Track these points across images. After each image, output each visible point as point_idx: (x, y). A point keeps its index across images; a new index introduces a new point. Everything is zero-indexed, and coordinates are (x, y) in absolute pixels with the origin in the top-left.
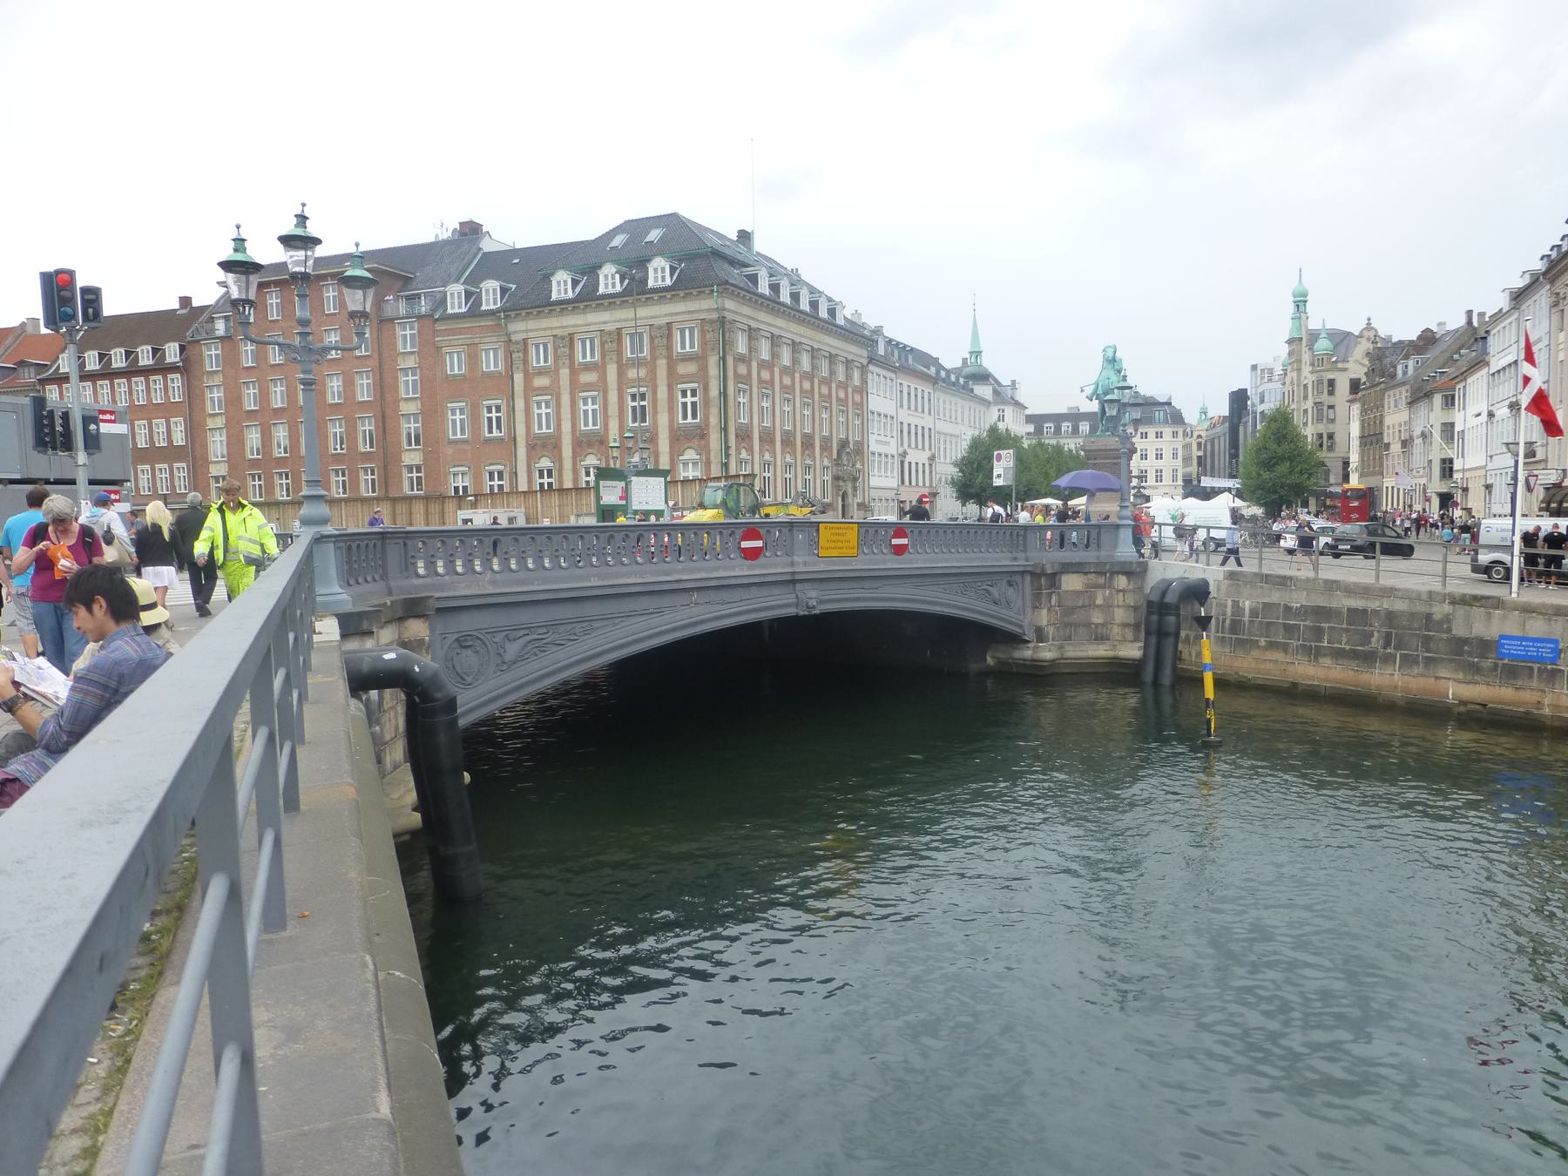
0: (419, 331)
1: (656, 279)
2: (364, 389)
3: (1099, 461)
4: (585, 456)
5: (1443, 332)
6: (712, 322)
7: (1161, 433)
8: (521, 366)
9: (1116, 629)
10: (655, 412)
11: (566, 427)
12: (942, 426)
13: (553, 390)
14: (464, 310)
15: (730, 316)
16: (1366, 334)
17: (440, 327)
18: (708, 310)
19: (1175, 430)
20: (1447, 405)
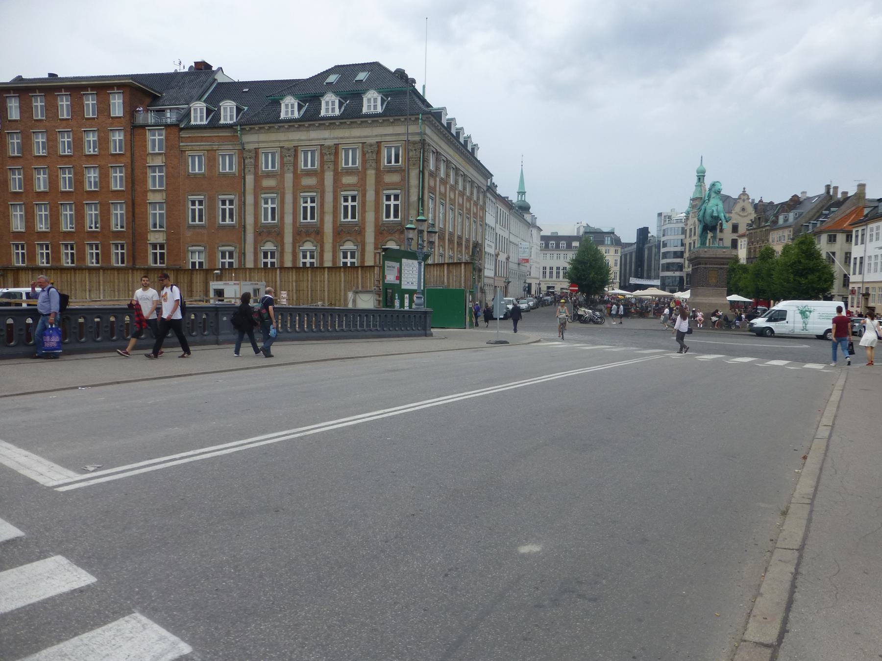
0: (166, 137)
1: (369, 107)
2: (117, 180)
3: (708, 266)
4: (304, 243)
5: (805, 198)
6: (414, 143)
7: (609, 250)
8: (252, 170)
10: (364, 211)
11: (288, 219)
12: (513, 239)
13: (280, 190)
14: (205, 122)
15: (428, 140)
16: (742, 197)
17: (184, 134)
19: (617, 249)
20: (830, 241)
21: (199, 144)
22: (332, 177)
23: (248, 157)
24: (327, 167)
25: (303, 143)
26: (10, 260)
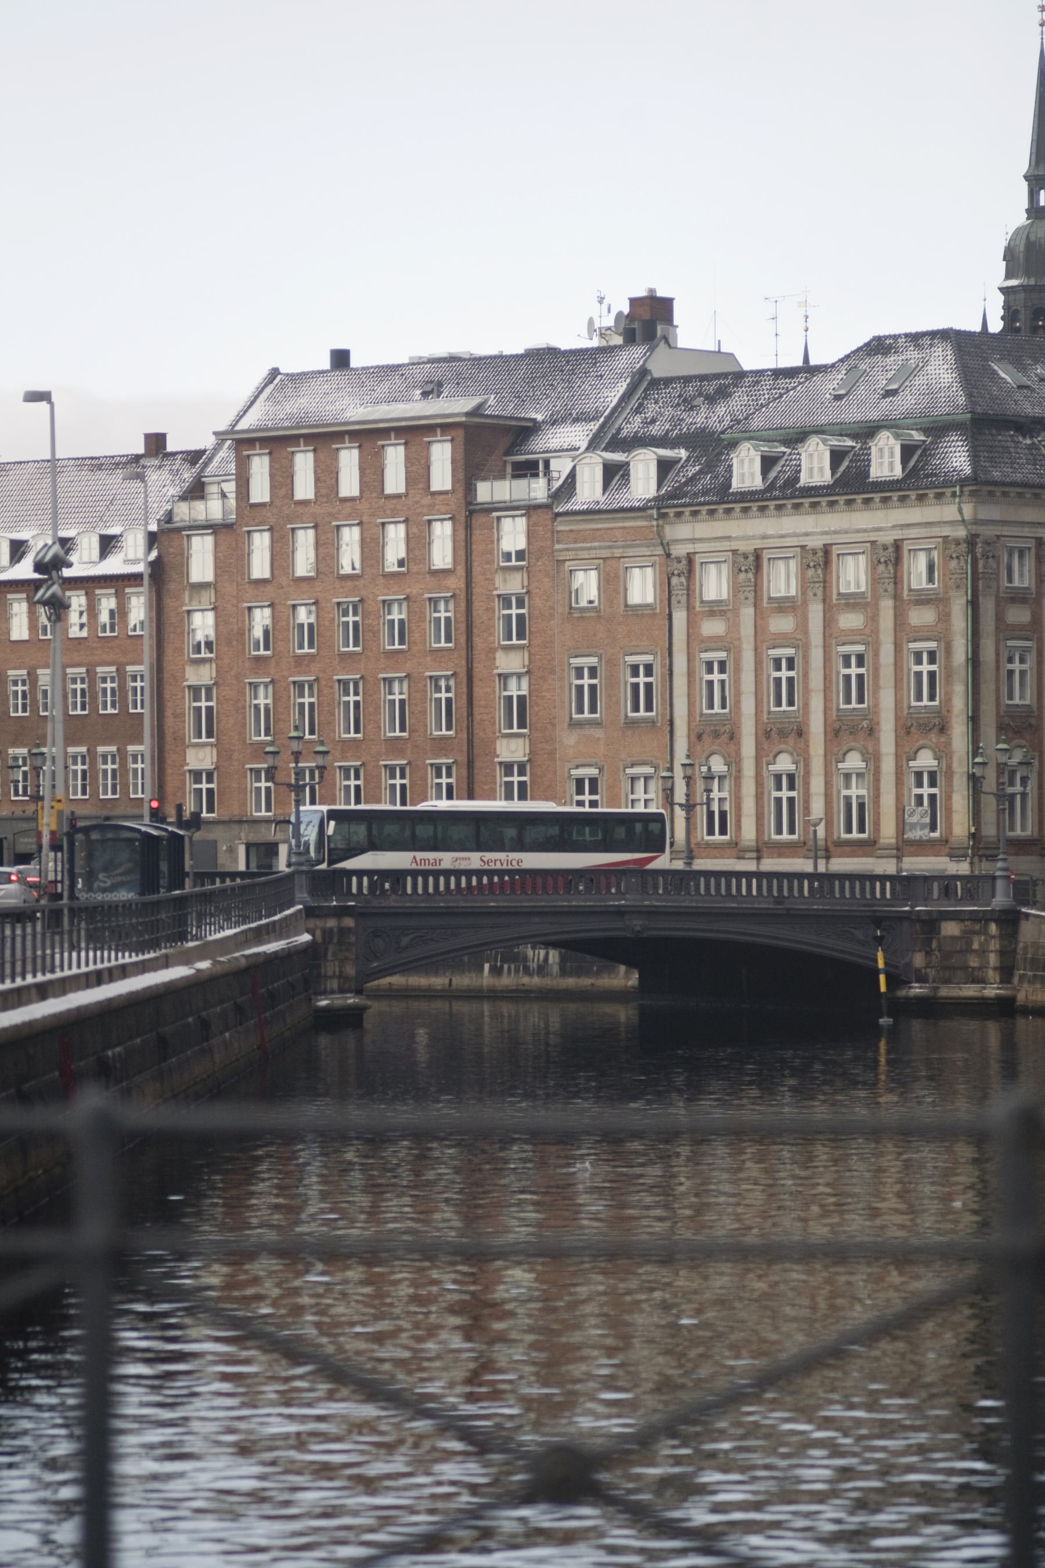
8: (684, 599)
9: (991, 973)
10: (877, 688)
17: (561, 526)
18: (952, 523)
21: (589, 545)
22: (821, 615)
23: (676, 572)
24: (742, 598)
25: (771, 543)
26: (244, 804)
